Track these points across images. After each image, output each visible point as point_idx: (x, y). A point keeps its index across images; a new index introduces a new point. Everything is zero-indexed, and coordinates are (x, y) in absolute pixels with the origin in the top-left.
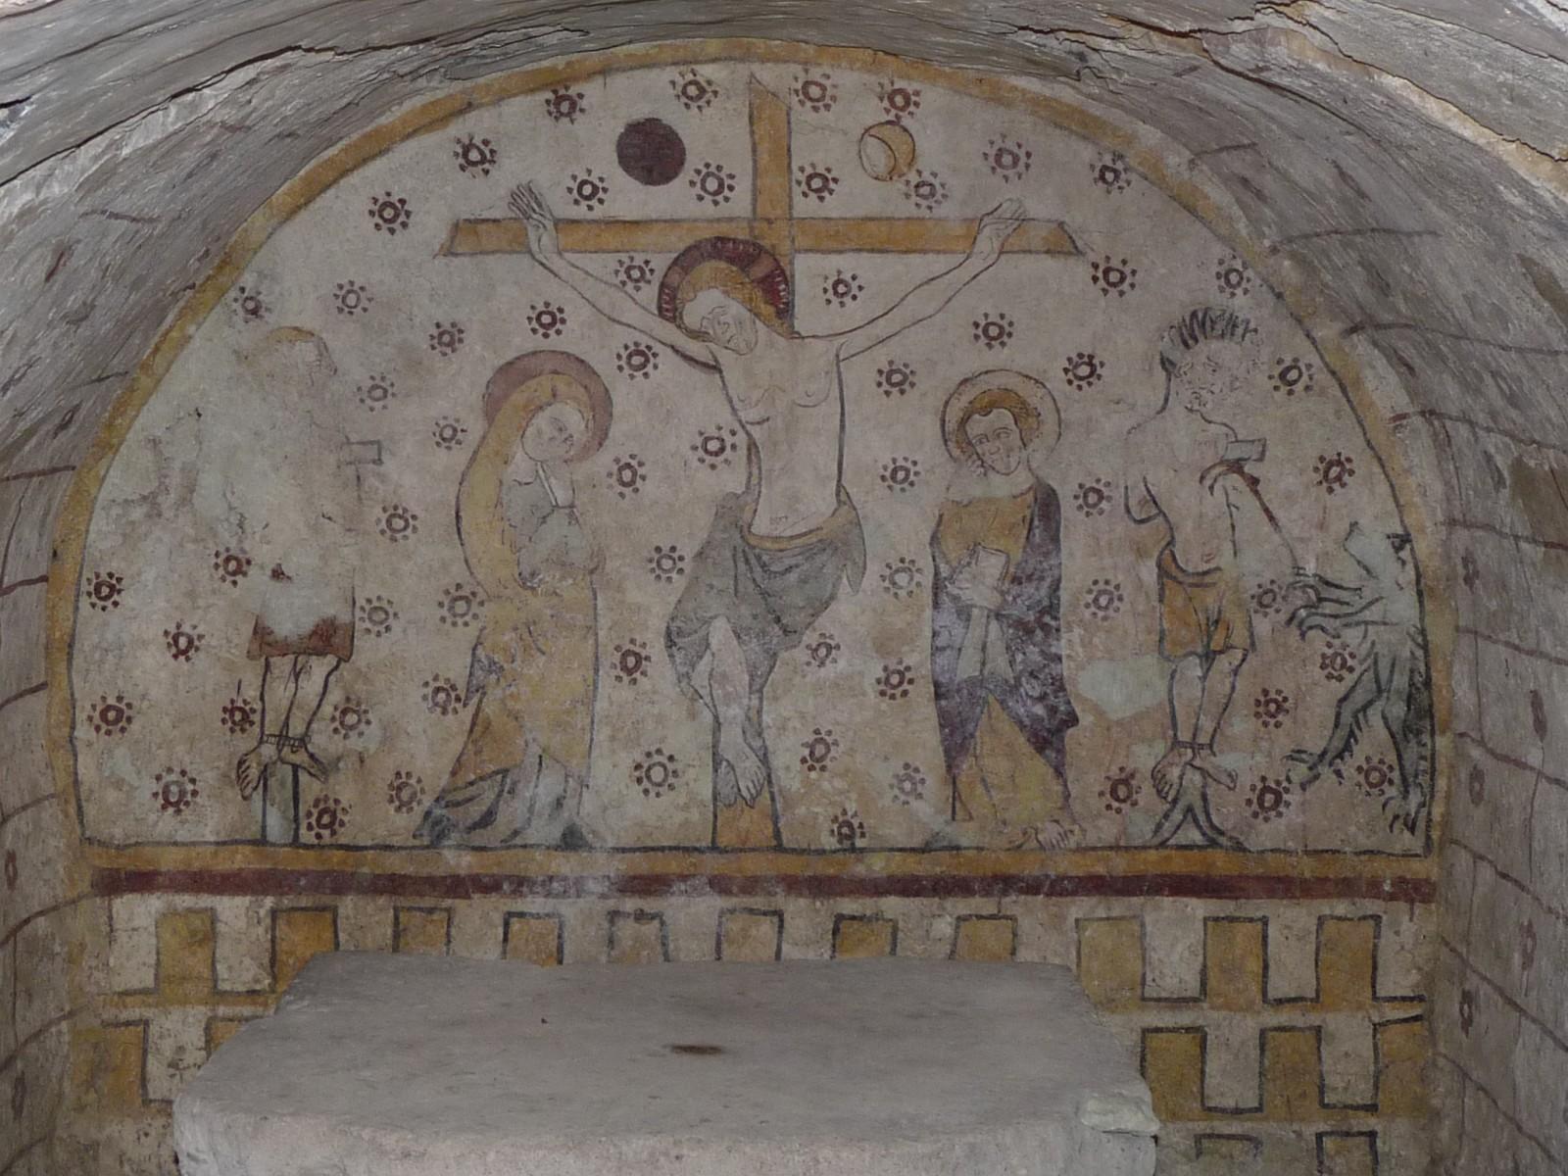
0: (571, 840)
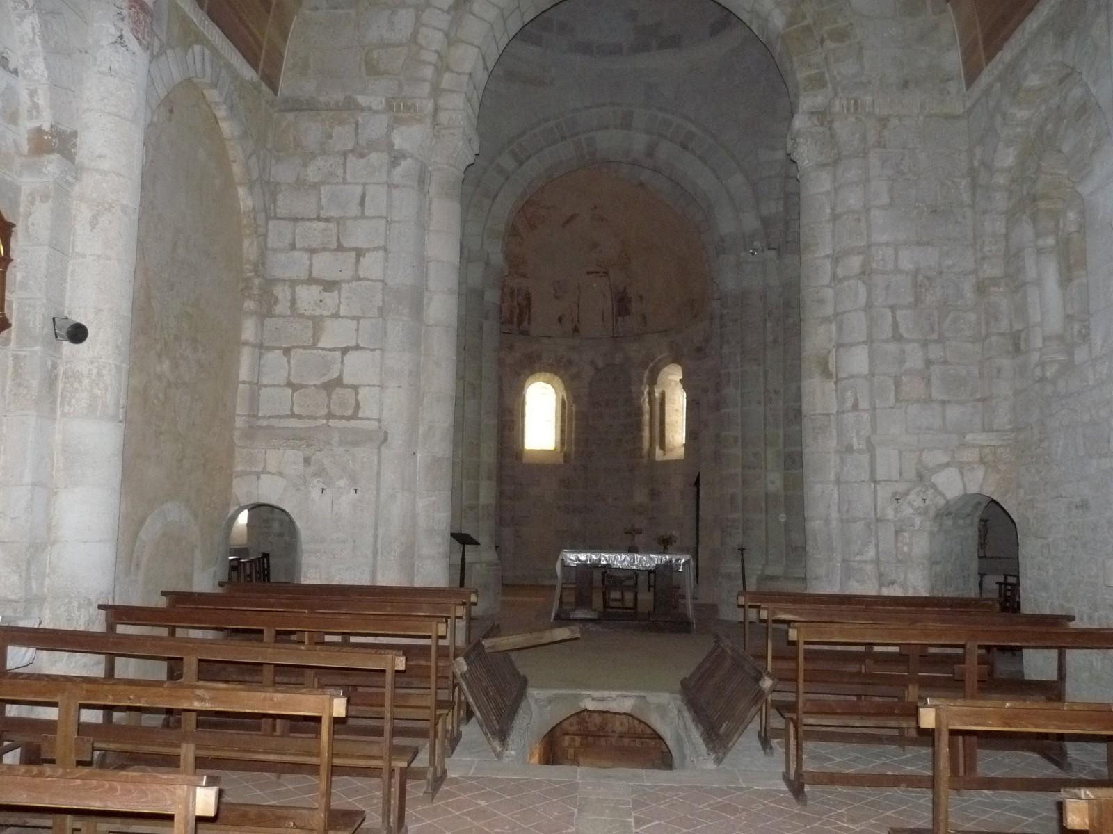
0: (613, 732)
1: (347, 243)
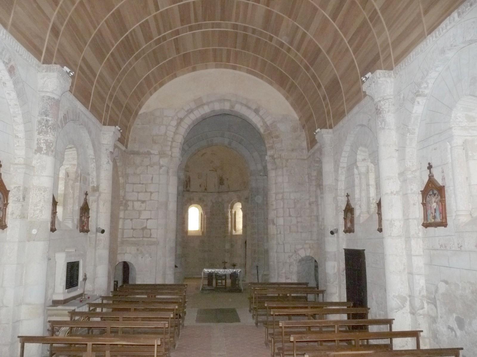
1: (148, 190)
